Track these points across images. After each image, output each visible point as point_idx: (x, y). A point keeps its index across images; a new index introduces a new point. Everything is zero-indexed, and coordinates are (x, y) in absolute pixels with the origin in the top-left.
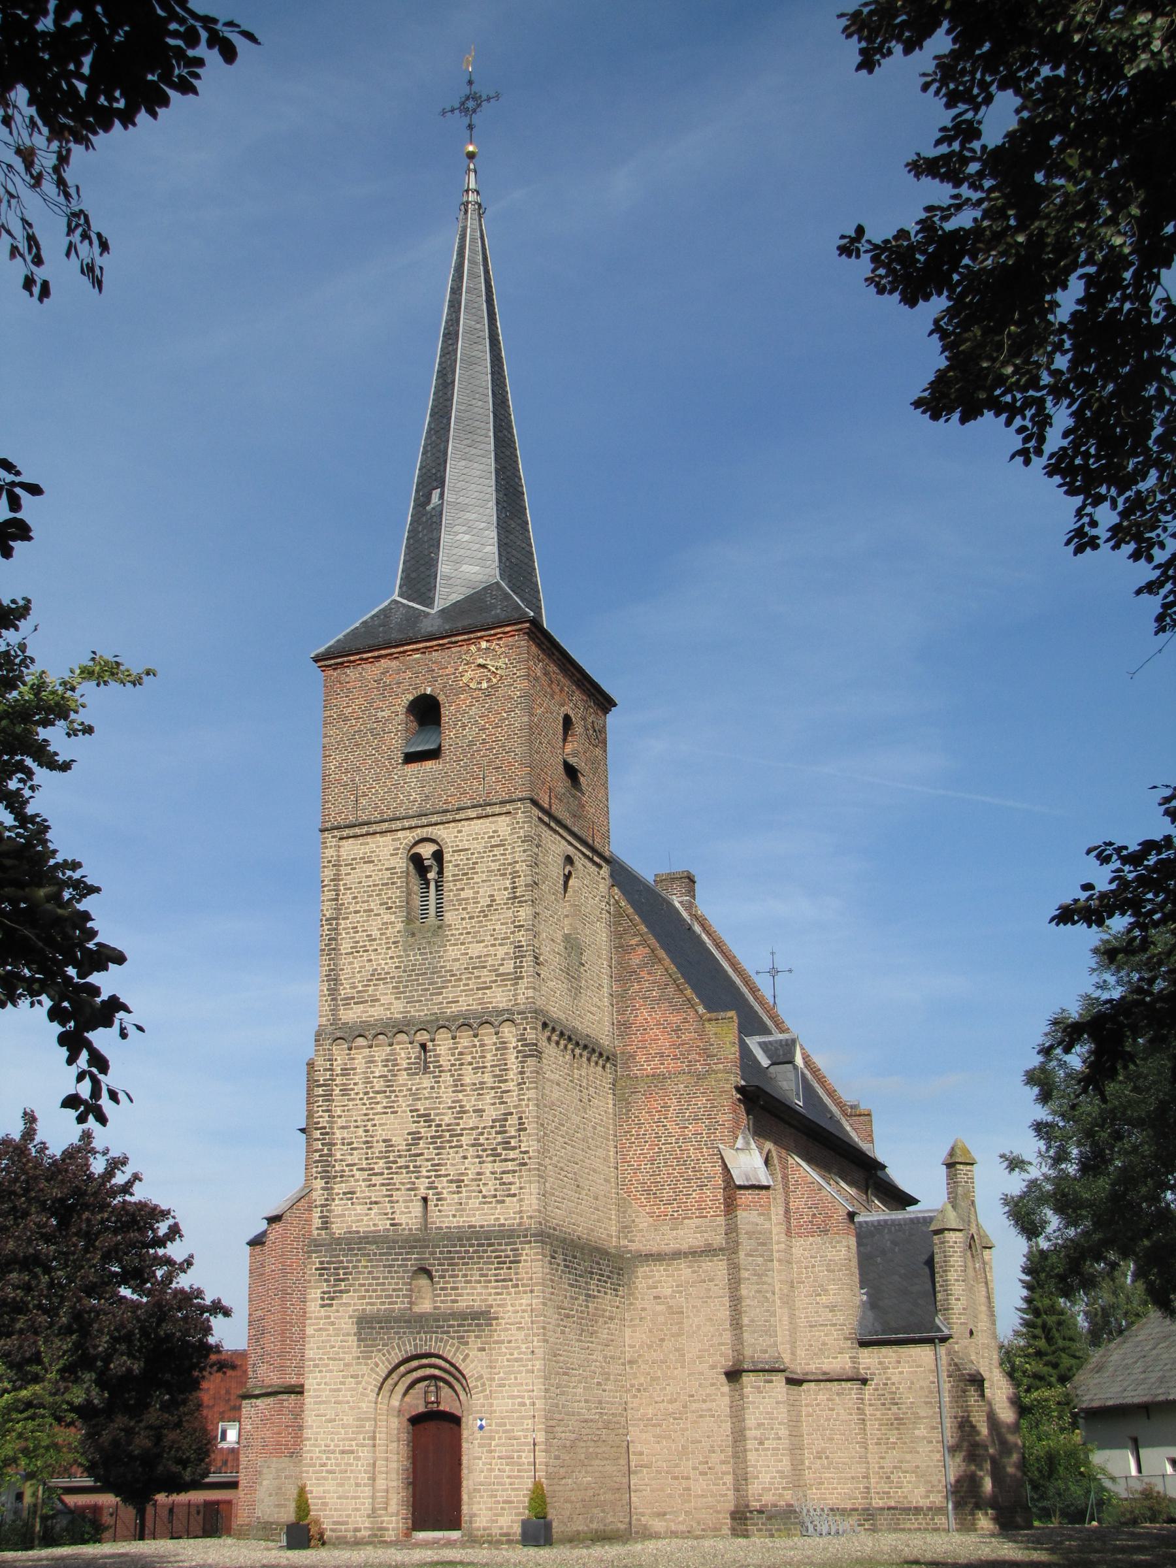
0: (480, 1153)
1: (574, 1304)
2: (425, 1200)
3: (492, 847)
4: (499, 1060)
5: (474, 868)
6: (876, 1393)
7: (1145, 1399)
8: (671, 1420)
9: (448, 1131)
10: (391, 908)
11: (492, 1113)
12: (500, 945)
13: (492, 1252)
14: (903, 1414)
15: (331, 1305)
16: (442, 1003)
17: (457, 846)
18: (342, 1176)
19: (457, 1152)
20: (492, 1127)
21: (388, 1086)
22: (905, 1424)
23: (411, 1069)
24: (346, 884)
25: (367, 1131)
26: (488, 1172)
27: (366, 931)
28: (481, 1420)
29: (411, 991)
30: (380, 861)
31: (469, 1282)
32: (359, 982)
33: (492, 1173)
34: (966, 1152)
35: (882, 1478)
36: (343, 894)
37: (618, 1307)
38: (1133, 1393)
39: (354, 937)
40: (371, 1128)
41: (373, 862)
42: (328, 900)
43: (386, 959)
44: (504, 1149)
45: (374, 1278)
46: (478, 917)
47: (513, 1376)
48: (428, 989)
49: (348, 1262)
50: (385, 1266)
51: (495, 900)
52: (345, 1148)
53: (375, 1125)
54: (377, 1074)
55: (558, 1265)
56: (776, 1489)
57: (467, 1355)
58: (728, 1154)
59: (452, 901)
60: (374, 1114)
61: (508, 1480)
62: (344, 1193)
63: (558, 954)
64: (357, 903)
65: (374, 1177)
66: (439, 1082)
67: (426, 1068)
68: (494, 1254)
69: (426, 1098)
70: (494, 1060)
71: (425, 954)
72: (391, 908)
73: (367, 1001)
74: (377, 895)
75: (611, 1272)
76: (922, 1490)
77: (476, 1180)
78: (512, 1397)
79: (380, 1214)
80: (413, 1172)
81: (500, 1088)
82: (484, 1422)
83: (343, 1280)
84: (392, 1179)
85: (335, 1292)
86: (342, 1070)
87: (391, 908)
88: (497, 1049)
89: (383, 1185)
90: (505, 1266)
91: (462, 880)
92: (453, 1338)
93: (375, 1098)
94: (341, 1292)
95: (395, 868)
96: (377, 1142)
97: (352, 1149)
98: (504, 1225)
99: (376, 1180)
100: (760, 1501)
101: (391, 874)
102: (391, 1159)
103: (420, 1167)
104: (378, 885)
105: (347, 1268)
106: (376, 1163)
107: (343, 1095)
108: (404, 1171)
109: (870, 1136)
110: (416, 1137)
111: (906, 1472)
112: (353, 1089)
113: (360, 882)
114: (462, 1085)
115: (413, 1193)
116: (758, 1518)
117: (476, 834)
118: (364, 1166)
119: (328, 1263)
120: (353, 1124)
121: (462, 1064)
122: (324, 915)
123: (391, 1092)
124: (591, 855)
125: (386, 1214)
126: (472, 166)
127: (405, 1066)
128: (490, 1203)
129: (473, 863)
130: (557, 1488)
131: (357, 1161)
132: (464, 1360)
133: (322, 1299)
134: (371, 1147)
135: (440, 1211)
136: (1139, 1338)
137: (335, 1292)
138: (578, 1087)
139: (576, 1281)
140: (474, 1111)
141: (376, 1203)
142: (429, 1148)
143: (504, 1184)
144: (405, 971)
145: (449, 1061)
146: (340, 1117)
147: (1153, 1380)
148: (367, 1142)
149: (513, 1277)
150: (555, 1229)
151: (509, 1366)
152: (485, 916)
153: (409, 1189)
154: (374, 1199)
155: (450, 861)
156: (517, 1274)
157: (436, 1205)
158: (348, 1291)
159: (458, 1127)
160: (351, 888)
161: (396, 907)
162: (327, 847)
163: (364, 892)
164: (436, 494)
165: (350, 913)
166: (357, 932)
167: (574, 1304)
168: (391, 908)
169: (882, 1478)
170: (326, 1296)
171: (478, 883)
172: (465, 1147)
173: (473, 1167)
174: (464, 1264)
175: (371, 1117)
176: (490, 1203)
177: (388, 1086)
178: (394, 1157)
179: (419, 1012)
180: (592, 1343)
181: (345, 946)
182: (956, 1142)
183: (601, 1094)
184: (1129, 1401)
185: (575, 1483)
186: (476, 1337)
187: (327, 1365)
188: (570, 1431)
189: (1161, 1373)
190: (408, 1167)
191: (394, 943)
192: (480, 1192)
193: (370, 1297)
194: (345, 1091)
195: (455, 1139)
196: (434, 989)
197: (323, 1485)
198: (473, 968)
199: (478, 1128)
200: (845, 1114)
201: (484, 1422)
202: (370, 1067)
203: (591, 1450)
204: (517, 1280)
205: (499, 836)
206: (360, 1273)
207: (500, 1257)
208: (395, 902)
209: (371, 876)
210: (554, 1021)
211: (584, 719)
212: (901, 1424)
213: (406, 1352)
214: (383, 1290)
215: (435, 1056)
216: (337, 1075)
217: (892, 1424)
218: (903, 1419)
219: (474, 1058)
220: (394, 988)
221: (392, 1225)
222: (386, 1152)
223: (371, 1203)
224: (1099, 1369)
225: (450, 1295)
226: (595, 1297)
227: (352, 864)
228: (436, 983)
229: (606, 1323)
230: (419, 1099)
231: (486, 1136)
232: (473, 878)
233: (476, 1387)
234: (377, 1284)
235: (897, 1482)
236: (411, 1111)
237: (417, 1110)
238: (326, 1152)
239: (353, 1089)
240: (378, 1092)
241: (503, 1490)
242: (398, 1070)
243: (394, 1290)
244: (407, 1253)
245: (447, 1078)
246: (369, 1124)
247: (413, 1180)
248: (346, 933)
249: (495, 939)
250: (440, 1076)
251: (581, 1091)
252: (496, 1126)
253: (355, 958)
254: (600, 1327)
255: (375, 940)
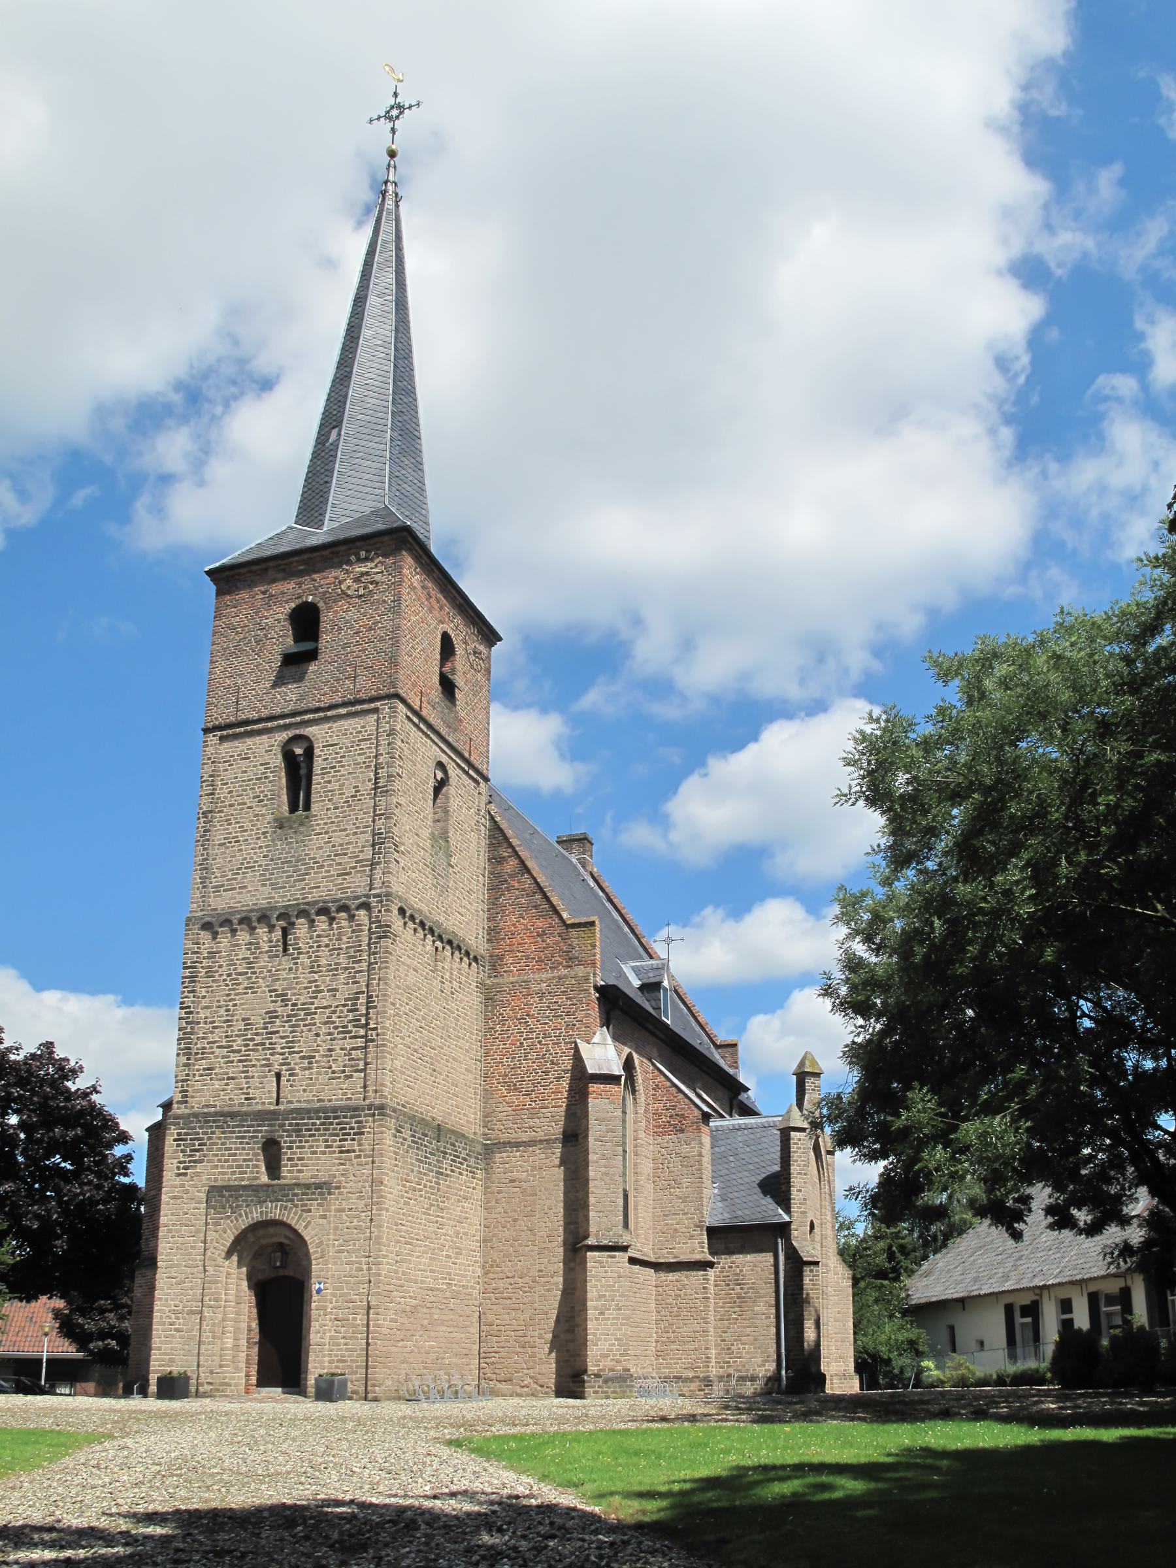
0: (332, 1030)
1: (422, 1179)
2: (278, 1076)
3: (359, 741)
4: (354, 942)
5: (341, 762)
6: (722, 1275)
7: (961, 1295)
8: (521, 1293)
9: (303, 1009)
10: (262, 801)
11: (345, 992)
12: (362, 833)
13: (338, 1124)
14: (745, 1293)
15: (185, 1174)
16: (304, 889)
17: (327, 741)
18: (203, 1053)
19: (310, 1030)
20: (344, 1006)
21: (250, 968)
22: (746, 1302)
23: (272, 951)
24: (222, 780)
25: (228, 1010)
26: (338, 1048)
27: (238, 822)
28: (320, 1283)
29: (276, 878)
30: (255, 757)
31: (315, 1153)
32: (230, 870)
33: (342, 1049)
34: (814, 1062)
35: (724, 1349)
36: (221, 789)
37: (474, 1188)
38: (952, 1291)
39: (228, 829)
40: (232, 1008)
41: (249, 758)
42: (207, 795)
43: (255, 848)
44: (355, 1026)
45: (227, 1149)
46: (342, 807)
47: (351, 1243)
48: (292, 876)
49: (204, 1133)
50: (237, 1138)
51: (359, 791)
52: (207, 1027)
53: (235, 1005)
54: (240, 957)
55: (405, 1139)
56: (615, 1355)
57: (309, 1222)
58: (583, 1048)
59: (319, 792)
60: (236, 995)
61: (342, 1341)
62: (204, 1069)
63: (423, 849)
64: (231, 797)
65: (232, 1054)
66: (297, 963)
67: (285, 950)
68: (339, 1127)
69: (284, 979)
70: (349, 942)
71: (291, 843)
72: (262, 801)
73: (234, 889)
74: (251, 789)
75: (467, 1155)
76: (759, 1360)
77: (326, 1056)
78: (352, 1263)
79: (237, 1089)
80: (269, 1049)
81: (354, 968)
82: (322, 1286)
83: (198, 1150)
84: (249, 1055)
85: (190, 1162)
86: (209, 953)
87: (262, 801)
88: (353, 932)
89: (240, 1061)
90: (349, 1137)
91: (330, 773)
92: (296, 1206)
93: (237, 979)
94: (195, 1162)
95: (268, 763)
96: (237, 1021)
97: (214, 1027)
98: (350, 1099)
99: (235, 1057)
100: (599, 1366)
101: (265, 769)
102: (249, 1037)
103: (275, 1044)
104: (252, 780)
105: (202, 1139)
106: (234, 1041)
107: (208, 977)
108: (260, 1048)
109: (736, 1062)
110: (273, 1015)
111: (745, 1344)
112: (217, 971)
113: (236, 778)
114: (319, 966)
115: (267, 1069)
116: (595, 1382)
117: (346, 730)
118: (224, 1044)
119: (186, 1134)
120: (216, 1004)
121: (319, 946)
122: (201, 809)
123: (252, 973)
124: (466, 768)
125: (241, 1089)
126: (392, 163)
127: (267, 949)
128: (339, 1078)
129: (341, 757)
130: (393, 1349)
131: (217, 1039)
132: (306, 1227)
133: (178, 1168)
134: (231, 1026)
135: (291, 1086)
136: (960, 1249)
137: (190, 1162)
138: (440, 978)
139: (426, 1157)
140: (329, 991)
141: (233, 1078)
142: (284, 1026)
143: (353, 1059)
144: (272, 860)
145: (308, 943)
146: (204, 997)
147: (967, 1281)
148: (228, 1021)
149: (357, 1148)
150: (403, 1106)
151: (348, 1234)
152: (350, 806)
153: (263, 1066)
154: (231, 1075)
155: (320, 756)
156: (360, 1145)
157: (288, 1080)
158: (201, 1161)
159: (313, 1006)
160: (227, 784)
161: (268, 800)
162: (207, 746)
163: (240, 786)
164: (334, 433)
165: (225, 807)
166: (230, 824)
167: (422, 1179)
168: (262, 801)
169: (724, 1349)
170: (182, 1165)
171: (344, 775)
172: (318, 1025)
173: (323, 1044)
174: (311, 1136)
175: (232, 997)
176: (339, 1078)
177: (250, 968)
178: (252, 1034)
179: (281, 899)
180: (442, 1217)
181: (218, 838)
182: (806, 1053)
183: (467, 990)
184: (949, 1297)
185: (414, 1346)
186: (319, 1205)
187: (180, 1231)
188: (411, 1297)
189: (976, 1275)
190: (264, 1044)
191: (264, 833)
192: (330, 1067)
193: (223, 1167)
194: (209, 974)
195: (309, 1017)
196: (298, 876)
197: (171, 1342)
198: (335, 855)
199: (331, 1006)
200: (717, 1047)
201: (322, 1286)
202: (234, 951)
203: (436, 1316)
204: (360, 1150)
205: (366, 731)
206: (213, 1144)
207: (345, 1129)
208: (266, 796)
209: (246, 772)
210: (414, 909)
211: (465, 643)
212: (743, 1302)
213: (253, 1218)
214: (234, 1161)
215: (295, 939)
216: (204, 958)
217: (735, 1302)
218: (744, 1298)
219: (331, 940)
220: (261, 875)
221: (246, 1099)
222: (245, 1030)
223: (229, 1078)
224: (927, 1274)
225: (297, 1165)
226: (447, 1175)
227: (230, 761)
228: (301, 870)
229: (459, 1201)
230: (278, 980)
231: (338, 1014)
232: (339, 771)
233: (316, 1252)
234: (230, 1155)
235: (737, 1353)
236: (270, 991)
237: (275, 990)
238: (189, 1030)
239: (217, 971)
240: (240, 974)
241: (338, 1350)
242: (260, 953)
243: (245, 1160)
244: (259, 1125)
245: (303, 959)
246: (231, 1003)
247: (268, 1056)
248: (221, 826)
249: (358, 828)
250: (298, 958)
251: (443, 983)
252: (347, 1005)
253: (227, 848)
254: (452, 1205)
255: (246, 831)
